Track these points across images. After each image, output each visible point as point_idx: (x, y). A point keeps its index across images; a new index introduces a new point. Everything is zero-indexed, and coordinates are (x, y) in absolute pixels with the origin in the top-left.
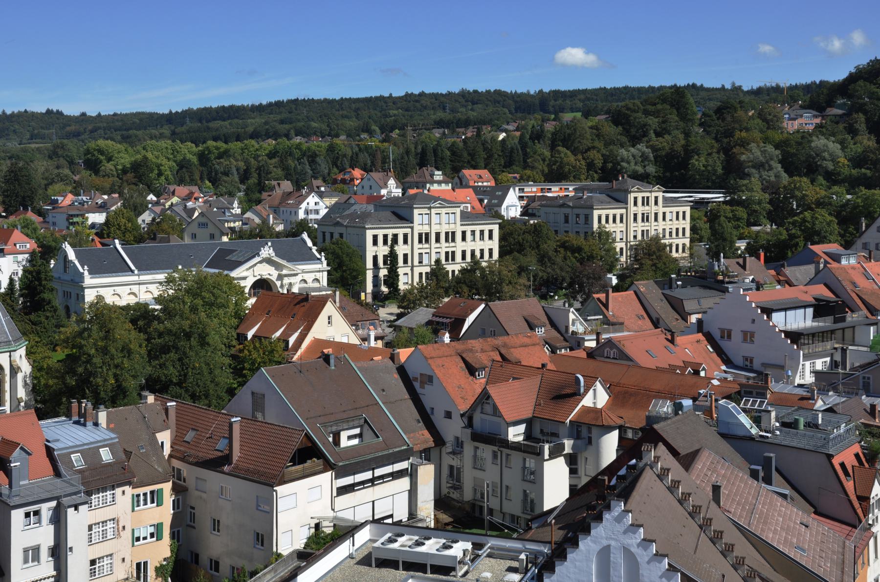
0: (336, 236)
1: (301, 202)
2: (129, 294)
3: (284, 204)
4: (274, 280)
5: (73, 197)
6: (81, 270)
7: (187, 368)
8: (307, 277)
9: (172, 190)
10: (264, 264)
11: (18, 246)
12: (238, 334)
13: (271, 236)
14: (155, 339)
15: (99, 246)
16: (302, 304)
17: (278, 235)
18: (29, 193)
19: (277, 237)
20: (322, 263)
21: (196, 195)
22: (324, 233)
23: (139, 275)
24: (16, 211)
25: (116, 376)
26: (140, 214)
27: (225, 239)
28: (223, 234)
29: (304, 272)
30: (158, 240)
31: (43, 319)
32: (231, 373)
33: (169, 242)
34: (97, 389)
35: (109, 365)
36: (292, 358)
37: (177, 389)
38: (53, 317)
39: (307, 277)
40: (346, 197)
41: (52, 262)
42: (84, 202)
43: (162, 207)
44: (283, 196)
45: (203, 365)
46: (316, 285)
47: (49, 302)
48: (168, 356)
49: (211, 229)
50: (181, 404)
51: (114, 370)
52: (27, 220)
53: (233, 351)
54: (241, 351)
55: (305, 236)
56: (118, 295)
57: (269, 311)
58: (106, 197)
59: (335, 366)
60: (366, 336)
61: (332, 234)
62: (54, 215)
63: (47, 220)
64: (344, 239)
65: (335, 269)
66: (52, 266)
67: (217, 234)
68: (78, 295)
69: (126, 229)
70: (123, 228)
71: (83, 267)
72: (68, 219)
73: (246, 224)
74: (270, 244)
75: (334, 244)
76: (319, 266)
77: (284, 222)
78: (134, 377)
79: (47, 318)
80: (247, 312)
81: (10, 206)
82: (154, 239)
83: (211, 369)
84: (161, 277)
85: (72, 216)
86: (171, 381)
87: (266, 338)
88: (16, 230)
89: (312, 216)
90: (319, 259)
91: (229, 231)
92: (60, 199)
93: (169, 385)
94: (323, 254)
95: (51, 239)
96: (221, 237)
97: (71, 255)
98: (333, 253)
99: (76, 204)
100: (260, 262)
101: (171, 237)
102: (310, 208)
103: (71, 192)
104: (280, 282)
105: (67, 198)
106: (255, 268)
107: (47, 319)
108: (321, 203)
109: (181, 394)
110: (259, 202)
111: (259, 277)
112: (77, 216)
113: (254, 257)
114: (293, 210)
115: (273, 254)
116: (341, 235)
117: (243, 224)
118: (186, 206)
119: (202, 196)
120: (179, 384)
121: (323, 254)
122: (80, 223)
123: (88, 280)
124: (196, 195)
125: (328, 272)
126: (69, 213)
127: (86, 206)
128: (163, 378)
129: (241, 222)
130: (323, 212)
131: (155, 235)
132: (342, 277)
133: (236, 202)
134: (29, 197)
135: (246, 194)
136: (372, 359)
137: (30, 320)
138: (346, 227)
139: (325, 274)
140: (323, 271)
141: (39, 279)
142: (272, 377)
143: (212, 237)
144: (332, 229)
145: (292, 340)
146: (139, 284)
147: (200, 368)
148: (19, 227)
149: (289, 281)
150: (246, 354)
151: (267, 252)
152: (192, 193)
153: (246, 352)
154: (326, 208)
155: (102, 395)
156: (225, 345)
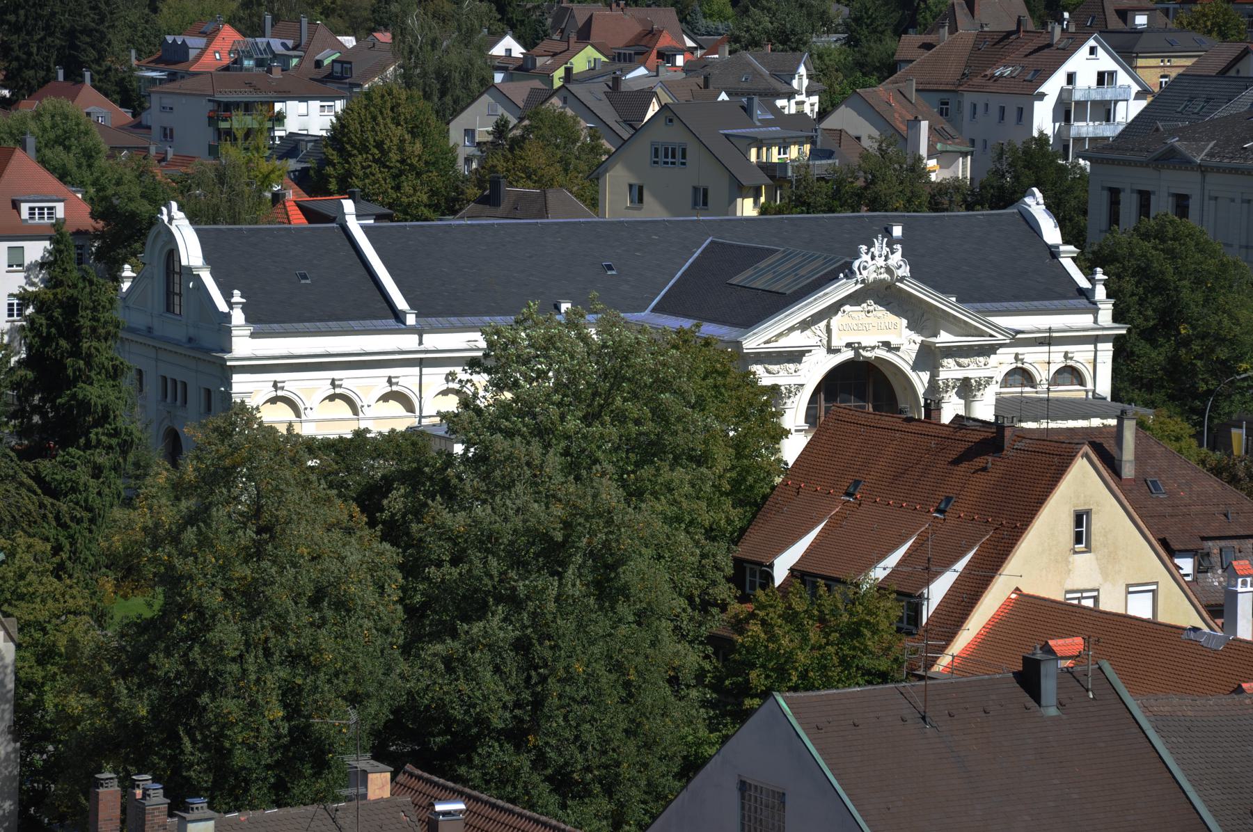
0: (1162, 206)
1: (1045, 74)
2: (385, 398)
3: (977, 80)
4: (907, 369)
5: (238, 37)
6: (222, 306)
7: (543, 679)
8: (1034, 358)
9: (581, 21)
10: (870, 305)
11: (25, 208)
12: (739, 563)
13: (910, 203)
14: (439, 564)
15: (298, 220)
16: (979, 462)
17: (940, 197)
18: (89, 21)
19: (935, 206)
20: (1093, 308)
21: (664, 42)
22: (1114, 193)
23: (419, 331)
24: (46, 81)
25: (290, 696)
26: (458, 108)
27: (747, 208)
28: (741, 190)
29: (1017, 339)
30: (505, 205)
31: (82, 475)
32: (705, 704)
33: (543, 212)
34: (220, 736)
35: (268, 653)
36: (933, 661)
37: (497, 753)
38: (116, 468)
39: (1034, 358)
40: (1228, 51)
41: (127, 272)
42: (275, 56)
43: (537, 84)
44: (976, 48)
45: (600, 668)
46: (1070, 391)
47: (104, 417)
48: (477, 628)
49: (697, 171)
50: (487, 811)
51: (283, 673)
52: (66, 117)
53: (717, 624)
54: (739, 625)
55: (1035, 204)
56: (344, 398)
57: (857, 483)
58: (349, 41)
59: (1060, 705)
60: (1219, 599)
61: (1145, 198)
62: (167, 101)
63: (146, 118)
64: (1193, 219)
65: (1148, 335)
66: (126, 286)
67: (718, 187)
68: (208, 392)
69: (403, 161)
70: (394, 156)
71: (227, 296)
72: (213, 121)
73: (829, 154)
74: (897, 231)
75: (1146, 236)
76: (1085, 320)
77: (972, 148)
78: (354, 699)
79: (97, 471)
80: (778, 480)
81: (27, 67)
82: (491, 200)
83: (627, 685)
84: (470, 341)
85: (228, 107)
86: (482, 721)
87: (831, 581)
88: (19, 152)
89: (1085, 128)
90: (1082, 293)
91: (763, 180)
92: (195, 43)
93: (478, 736)
94: (1100, 275)
95: (136, 190)
96: (732, 202)
97: (190, 249)
98: (1142, 272)
99: (248, 63)
100: (854, 299)
101: (551, 194)
102: (1078, 96)
103: (233, 21)
104: (925, 376)
105: (217, 43)
106: (836, 321)
107: (96, 476)
108: (1123, 78)
109: (517, 772)
110: (888, 69)
111: (848, 354)
112: (248, 107)
113: (831, 278)
114: (1011, 106)
115: (905, 271)
116: (1182, 204)
117: (815, 154)
118: (616, 81)
119: (690, 43)
120: (516, 736)
121: (1100, 275)
122: (240, 135)
123: (244, 345)
124: (664, 42)
125: (1118, 342)
126: (219, 97)
127: (277, 73)
128: (457, 713)
129: (807, 148)
130: (1128, 111)
131: (495, 184)
132: (1175, 369)
133: (802, 70)
134: (87, 31)
135: (852, 41)
136: (1239, 690)
137: (38, 478)
138: (1203, 169)
139: (1106, 351)
140: (1095, 340)
141: (73, 334)
142: (816, 730)
143: (701, 198)
144: (1145, 179)
145: (938, 590)
146: (421, 363)
147: (591, 677)
148: (31, 142)
149: (961, 374)
150: (755, 638)
151: (880, 262)
152: (651, 34)
153: (755, 628)
154: (1139, 96)
155: (240, 758)
156: (690, 599)
